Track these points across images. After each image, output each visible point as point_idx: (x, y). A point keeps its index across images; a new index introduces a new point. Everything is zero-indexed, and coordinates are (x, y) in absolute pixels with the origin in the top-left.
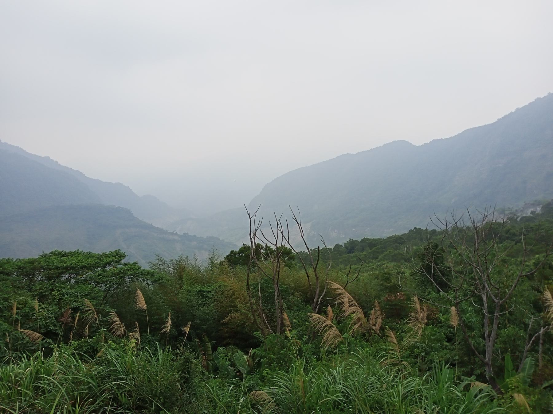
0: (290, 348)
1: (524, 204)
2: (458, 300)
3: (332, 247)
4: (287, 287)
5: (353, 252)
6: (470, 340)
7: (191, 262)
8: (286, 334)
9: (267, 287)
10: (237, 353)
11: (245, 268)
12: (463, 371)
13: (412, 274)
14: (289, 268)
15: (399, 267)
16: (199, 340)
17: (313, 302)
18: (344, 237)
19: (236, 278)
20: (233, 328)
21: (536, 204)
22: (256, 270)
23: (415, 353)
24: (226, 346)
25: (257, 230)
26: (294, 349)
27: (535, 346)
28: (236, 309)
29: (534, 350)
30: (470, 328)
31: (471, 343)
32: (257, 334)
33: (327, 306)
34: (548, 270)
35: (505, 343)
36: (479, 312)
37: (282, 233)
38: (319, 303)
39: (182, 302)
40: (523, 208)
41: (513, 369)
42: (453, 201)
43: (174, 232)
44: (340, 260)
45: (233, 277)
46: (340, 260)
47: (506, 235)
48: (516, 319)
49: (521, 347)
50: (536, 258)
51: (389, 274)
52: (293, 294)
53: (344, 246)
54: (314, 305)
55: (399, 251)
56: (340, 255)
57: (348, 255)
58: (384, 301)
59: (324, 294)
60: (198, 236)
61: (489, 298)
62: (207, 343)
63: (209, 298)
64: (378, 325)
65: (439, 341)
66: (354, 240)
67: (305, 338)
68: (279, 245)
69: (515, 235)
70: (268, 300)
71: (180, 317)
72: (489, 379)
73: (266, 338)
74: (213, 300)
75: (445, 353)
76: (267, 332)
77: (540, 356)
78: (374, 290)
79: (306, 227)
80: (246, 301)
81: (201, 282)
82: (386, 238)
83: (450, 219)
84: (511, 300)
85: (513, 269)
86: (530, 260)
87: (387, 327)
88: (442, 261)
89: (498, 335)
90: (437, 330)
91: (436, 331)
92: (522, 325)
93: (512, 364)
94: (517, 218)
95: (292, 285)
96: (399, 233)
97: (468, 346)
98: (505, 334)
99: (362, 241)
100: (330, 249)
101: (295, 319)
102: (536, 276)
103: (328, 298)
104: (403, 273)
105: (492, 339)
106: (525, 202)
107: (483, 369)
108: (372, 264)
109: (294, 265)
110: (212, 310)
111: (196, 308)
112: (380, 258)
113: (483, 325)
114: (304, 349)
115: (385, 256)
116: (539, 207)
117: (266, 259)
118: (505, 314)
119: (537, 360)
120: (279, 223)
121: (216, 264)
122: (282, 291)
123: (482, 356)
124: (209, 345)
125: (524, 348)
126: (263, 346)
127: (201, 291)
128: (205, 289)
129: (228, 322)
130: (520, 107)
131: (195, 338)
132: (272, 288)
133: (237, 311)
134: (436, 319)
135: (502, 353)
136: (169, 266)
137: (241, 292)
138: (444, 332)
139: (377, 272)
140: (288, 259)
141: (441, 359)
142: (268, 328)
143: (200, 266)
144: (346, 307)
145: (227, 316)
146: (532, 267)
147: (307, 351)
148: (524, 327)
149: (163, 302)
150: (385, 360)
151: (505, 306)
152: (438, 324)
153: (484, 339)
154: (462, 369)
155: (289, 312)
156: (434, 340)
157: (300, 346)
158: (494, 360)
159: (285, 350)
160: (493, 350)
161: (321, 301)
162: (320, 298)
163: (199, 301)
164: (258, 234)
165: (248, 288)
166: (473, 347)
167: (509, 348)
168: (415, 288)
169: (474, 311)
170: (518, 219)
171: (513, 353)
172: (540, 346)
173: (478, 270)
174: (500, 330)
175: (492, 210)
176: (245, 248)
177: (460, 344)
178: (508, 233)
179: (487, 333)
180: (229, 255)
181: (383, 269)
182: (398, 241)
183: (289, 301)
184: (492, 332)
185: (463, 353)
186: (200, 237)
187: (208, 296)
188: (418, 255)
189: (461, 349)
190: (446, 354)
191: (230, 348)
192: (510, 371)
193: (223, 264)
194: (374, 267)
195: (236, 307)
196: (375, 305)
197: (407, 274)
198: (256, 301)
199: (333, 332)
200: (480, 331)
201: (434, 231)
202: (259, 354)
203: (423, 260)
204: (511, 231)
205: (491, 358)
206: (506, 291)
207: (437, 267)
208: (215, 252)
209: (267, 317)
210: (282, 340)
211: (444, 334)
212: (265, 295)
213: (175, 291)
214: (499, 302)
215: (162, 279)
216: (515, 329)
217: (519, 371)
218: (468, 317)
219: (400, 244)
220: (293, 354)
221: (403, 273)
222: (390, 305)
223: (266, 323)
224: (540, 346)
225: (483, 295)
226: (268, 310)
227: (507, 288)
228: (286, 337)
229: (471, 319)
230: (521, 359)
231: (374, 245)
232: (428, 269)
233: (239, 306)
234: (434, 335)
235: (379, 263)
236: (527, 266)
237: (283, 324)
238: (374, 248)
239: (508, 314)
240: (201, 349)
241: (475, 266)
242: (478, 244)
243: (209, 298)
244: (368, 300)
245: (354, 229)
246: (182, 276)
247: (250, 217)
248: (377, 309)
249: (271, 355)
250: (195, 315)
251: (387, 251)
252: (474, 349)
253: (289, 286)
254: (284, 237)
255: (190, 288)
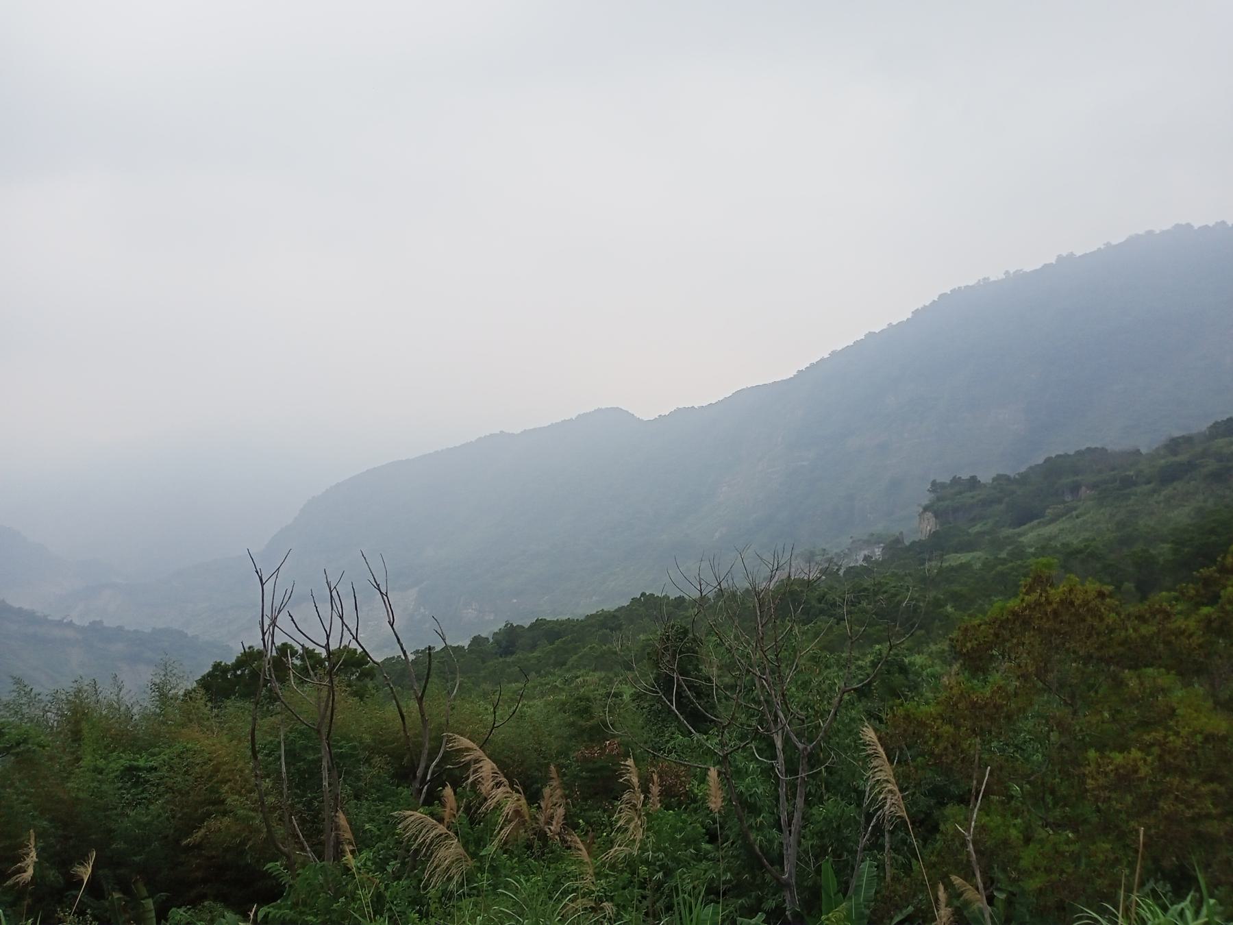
0: (355, 893)
1: (851, 540)
2: (728, 749)
3: (465, 643)
4: (355, 746)
5: (512, 653)
6: (753, 836)
7: (107, 692)
8: (346, 862)
9: (306, 748)
10: (222, 919)
11: (249, 705)
12: (742, 906)
13: (637, 697)
14: (361, 698)
15: (611, 681)
16: (124, 893)
17: (415, 777)
18: (492, 618)
19: (225, 732)
20: (213, 857)
21: (871, 541)
22: (279, 709)
23: (641, 876)
24: (194, 902)
25: (279, 613)
26: (366, 896)
27: (878, 838)
28: (222, 808)
29: (875, 846)
30: (754, 809)
31: (756, 840)
32: (273, 866)
33: (444, 786)
34: (897, 675)
35: (820, 835)
36: (768, 772)
37: (341, 618)
38: (428, 778)
39: (77, 799)
40: (849, 549)
41: (839, 892)
42: (717, 535)
43: (64, 618)
44: (483, 673)
45: (216, 730)
46: (483, 673)
47: (819, 605)
48: (840, 782)
49: (853, 842)
50: (875, 651)
51: (588, 699)
52: (367, 761)
53: (491, 640)
54: (417, 786)
55: (610, 646)
56: (484, 662)
57: (501, 660)
58: (577, 761)
59: (440, 755)
60: (127, 628)
61: (787, 740)
62: (143, 899)
63: (153, 785)
64: (557, 823)
65: (688, 842)
66: (515, 625)
67: (392, 866)
68: (332, 648)
69: (834, 605)
70: (306, 779)
71: (71, 838)
72: (792, 917)
73: (298, 875)
74: (162, 788)
75: (703, 867)
76: (302, 858)
77: (887, 856)
78: (556, 738)
79: (403, 601)
80: (248, 786)
81: (132, 746)
82: (583, 618)
83: (708, 576)
84: (829, 743)
85: (829, 676)
86: (865, 655)
87: (581, 821)
88: (697, 665)
89: (806, 818)
90: (688, 819)
91: (684, 822)
92: (853, 795)
93: (835, 879)
94: (838, 570)
95: (367, 739)
96: (610, 606)
97: (748, 847)
98: (821, 815)
99: (533, 626)
100: (460, 648)
101: (371, 820)
102: (876, 689)
103: (448, 766)
104: (618, 695)
105: (796, 829)
106: (851, 537)
107: (780, 897)
108: (554, 678)
109: (373, 691)
110: (159, 816)
111: (115, 812)
112: (569, 663)
113: (777, 799)
114: (387, 894)
115: (581, 658)
116: (879, 548)
117: (302, 682)
118: (820, 772)
119: (880, 867)
120: (334, 593)
121: (172, 699)
122: (341, 756)
123: (778, 867)
124: (150, 904)
125: (857, 843)
126: (289, 894)
127: (131, 769)
128: (141, 763)
129: (201, 842)
130: (839, 348)
131: (114, 890)
132: (316, 750)
133: (225, 813)
134: (686, 794)
135: (816, 858)
136: (47, 708)
137: (236, 765)
138: (702, 821)
139: (563, 697)
140: (358, 678)
141: (697, 882)
142: (303, 849)
143: (130, 706)
144: (485, 787)
145: (200, 827)
146: (869, 671)
147: (396, 898)
148: (855, 797)
149: (25, 802)
150: (572, 900)
151: (818, 755)
152: (690, 804)
153: (780, 830)
154: (740, 901)
155: (356, 804)
156: (682, 840)
157: (377, 887)
158: (801, 874)
159: (343, 899)
160: (798, 853)
161: (433, 774)
162: (432, 767)
163: (123, 793)
164: (283, 620)
165: (254, 754)
166: (757, 848)
167: (830, 846)
168: (643, 728)
169: (759, 769)
170: (841, 573)
171: (837, 855)
172: (887, 836)
173: (764, 681)
174: (811, 808)
175: (787, 555)
176: (249, 657)
177: (734, 846)
178: (823, 602)
179: (784, 817)
180: (209, 675)
181: (577, 688)
182: (607, 623)
183: (358, 779)
184: (795, 814)
185: (740, 864)
186: (136, 631)
187: (149, 781)
188: (648, 654)
189: (737, 857)
190: (706, 871)
191: (204, 907)
192: (833, 897)
193: (191, 698)
194: (557, 684)
195: (223, 802)
196: (551, 776)
197: (626, 697)
198: (274, 784)
199: (451, 850)
200: (773, 813)
201: (681, 600)
202: (278, 916)
203: (656, 665)
204: (828, 596)
205: (793, 871)
206: (820, 723)
207: (684, 680)
208: (170, 668)
209: (302, 822)
210: (337, 876)
211: (703, 826)
212: (297, 769)
213: (60, 771)
214: (806, 749)
215: (25, 741)
216: (839, 803)
217: (849, 894)
218: (748, 784)
219: (612, 629)
220: (360, 909)
221: (618, 695)
222: (590, 771)
223: (298, 836)
224: (887, 836)
225: (775, 736)
226: (304, 806)
227: (822, 716)
228: (347, 869)
229: (754, 789)
230: (853, 869)
231: (558, 635)
232: (666, 683)
233: (231, 800)
234: (681, 830)
235: (568, 676)
236: (860, 668)
237: (338, 843)
238: (557, 642)
239: (826, 771)
240: (127, 916)
241: (759, 674)
242: (762, 627)
243: (153, 785)
244: (542, 761)
245: (515, 601)
246: (80, 731)
247: (261, 580)
248: (555, 783)
249: (309, 915)
250: (114, 831)
251: (584, 648)
252: (760, 854)
253: (361, 743)
254: (346, 626)
255: (101, 763)
